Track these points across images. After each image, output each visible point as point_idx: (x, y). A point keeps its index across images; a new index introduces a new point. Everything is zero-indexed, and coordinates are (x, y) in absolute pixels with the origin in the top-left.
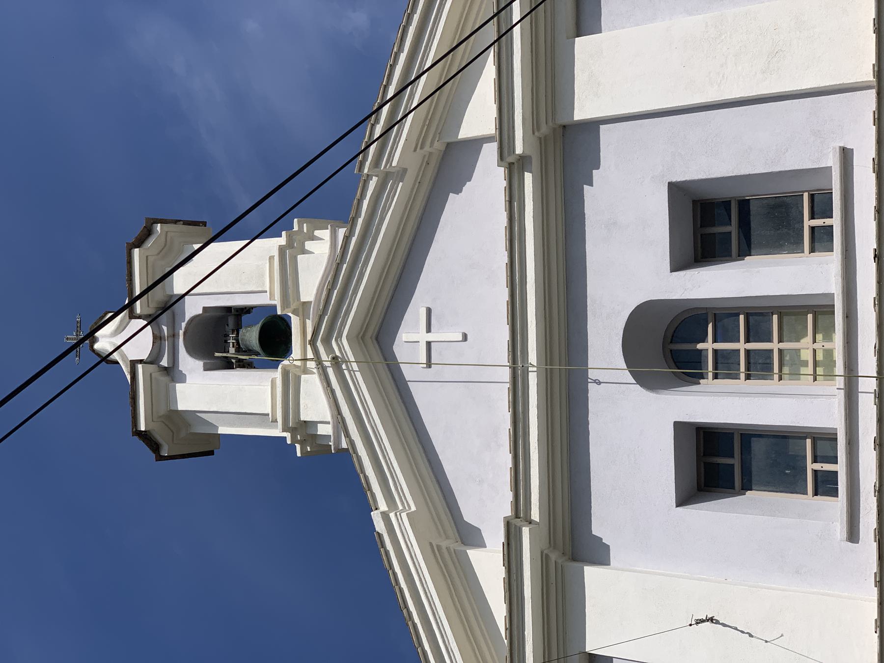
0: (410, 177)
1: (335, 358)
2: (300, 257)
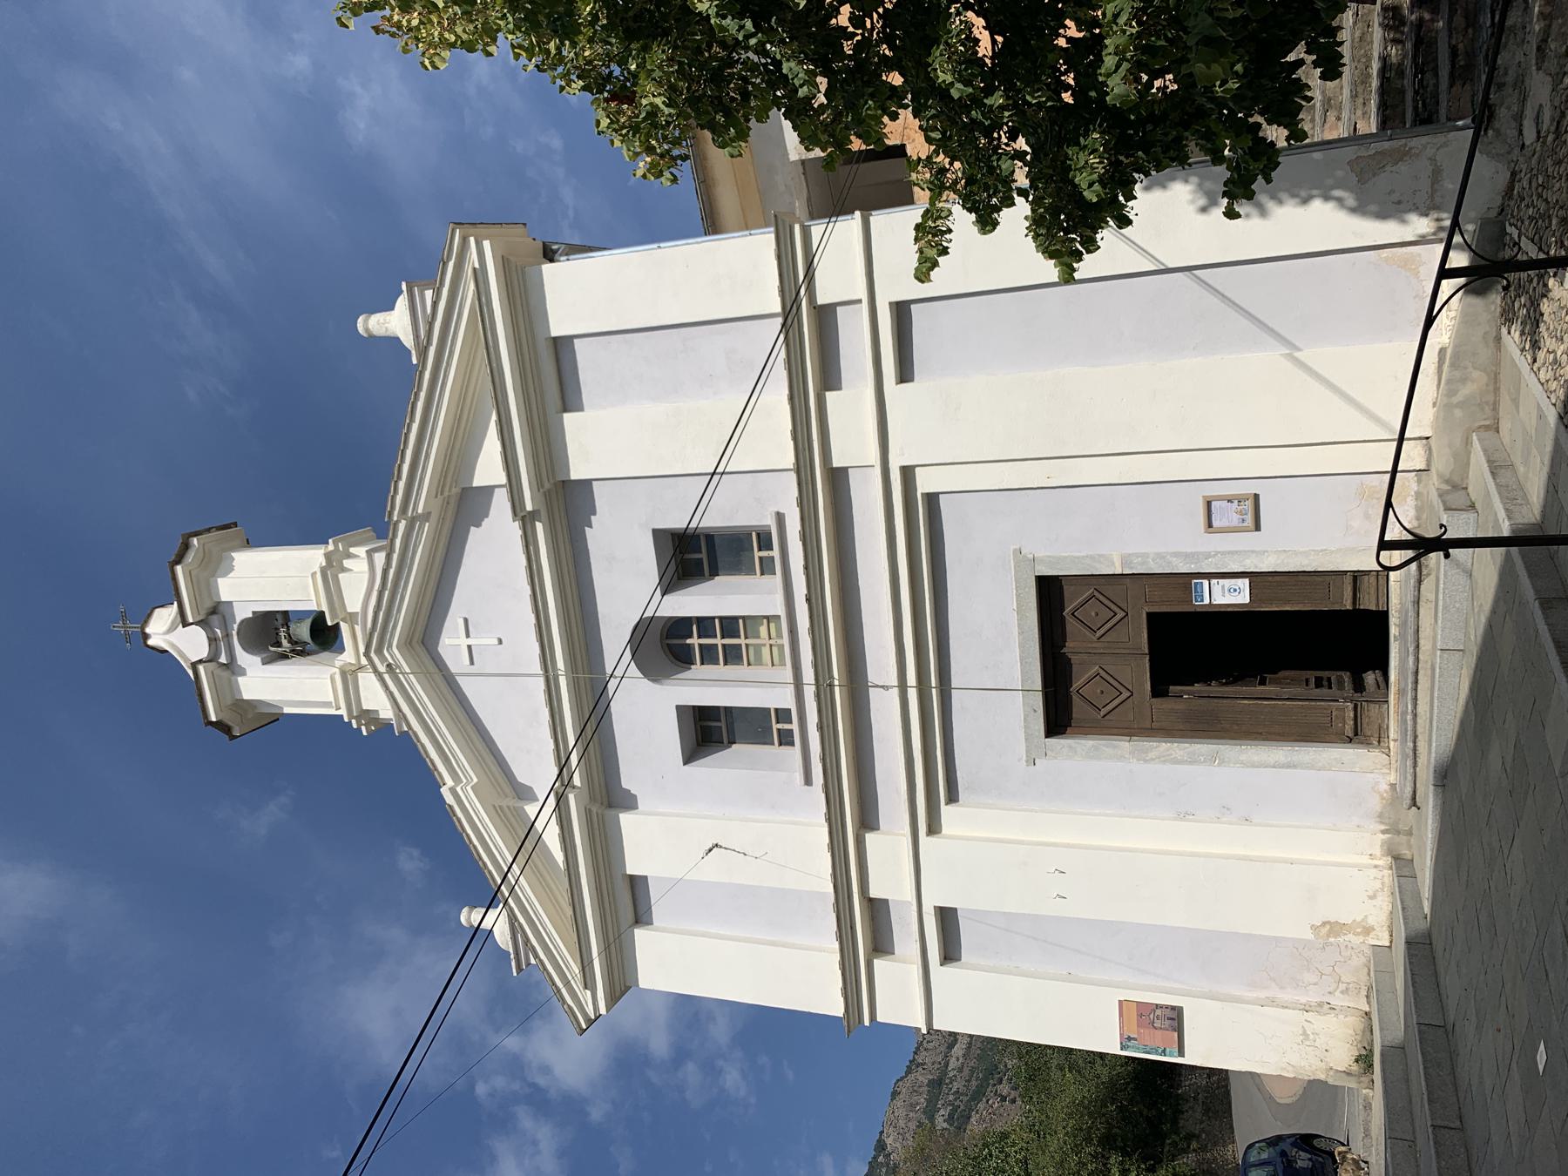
0: (434, 517)
1: (389, 665)
2: (340, 576)
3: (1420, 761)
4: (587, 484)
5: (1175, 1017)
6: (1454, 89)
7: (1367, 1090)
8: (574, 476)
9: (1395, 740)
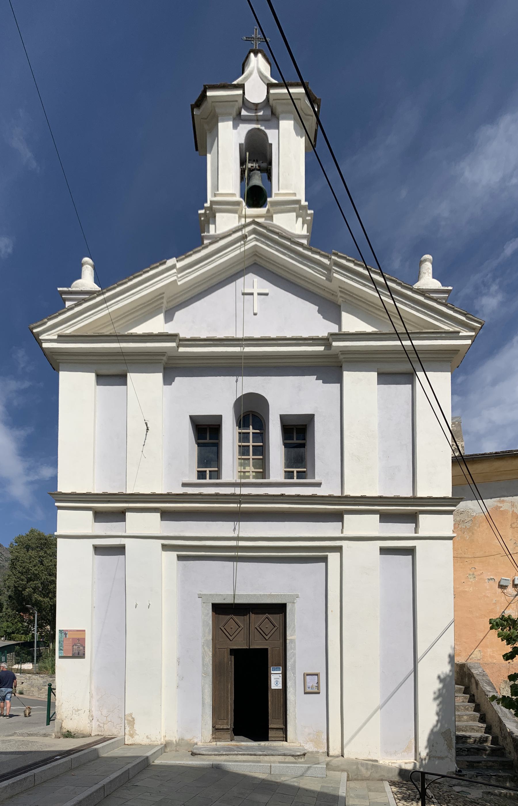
0: (327, 284)
3: (217, 757)
4: (339, 380)
5: (80, 655)
6: (466, 762)
7: (54, 736)
8: (346, 374)
9: (216, 745)
